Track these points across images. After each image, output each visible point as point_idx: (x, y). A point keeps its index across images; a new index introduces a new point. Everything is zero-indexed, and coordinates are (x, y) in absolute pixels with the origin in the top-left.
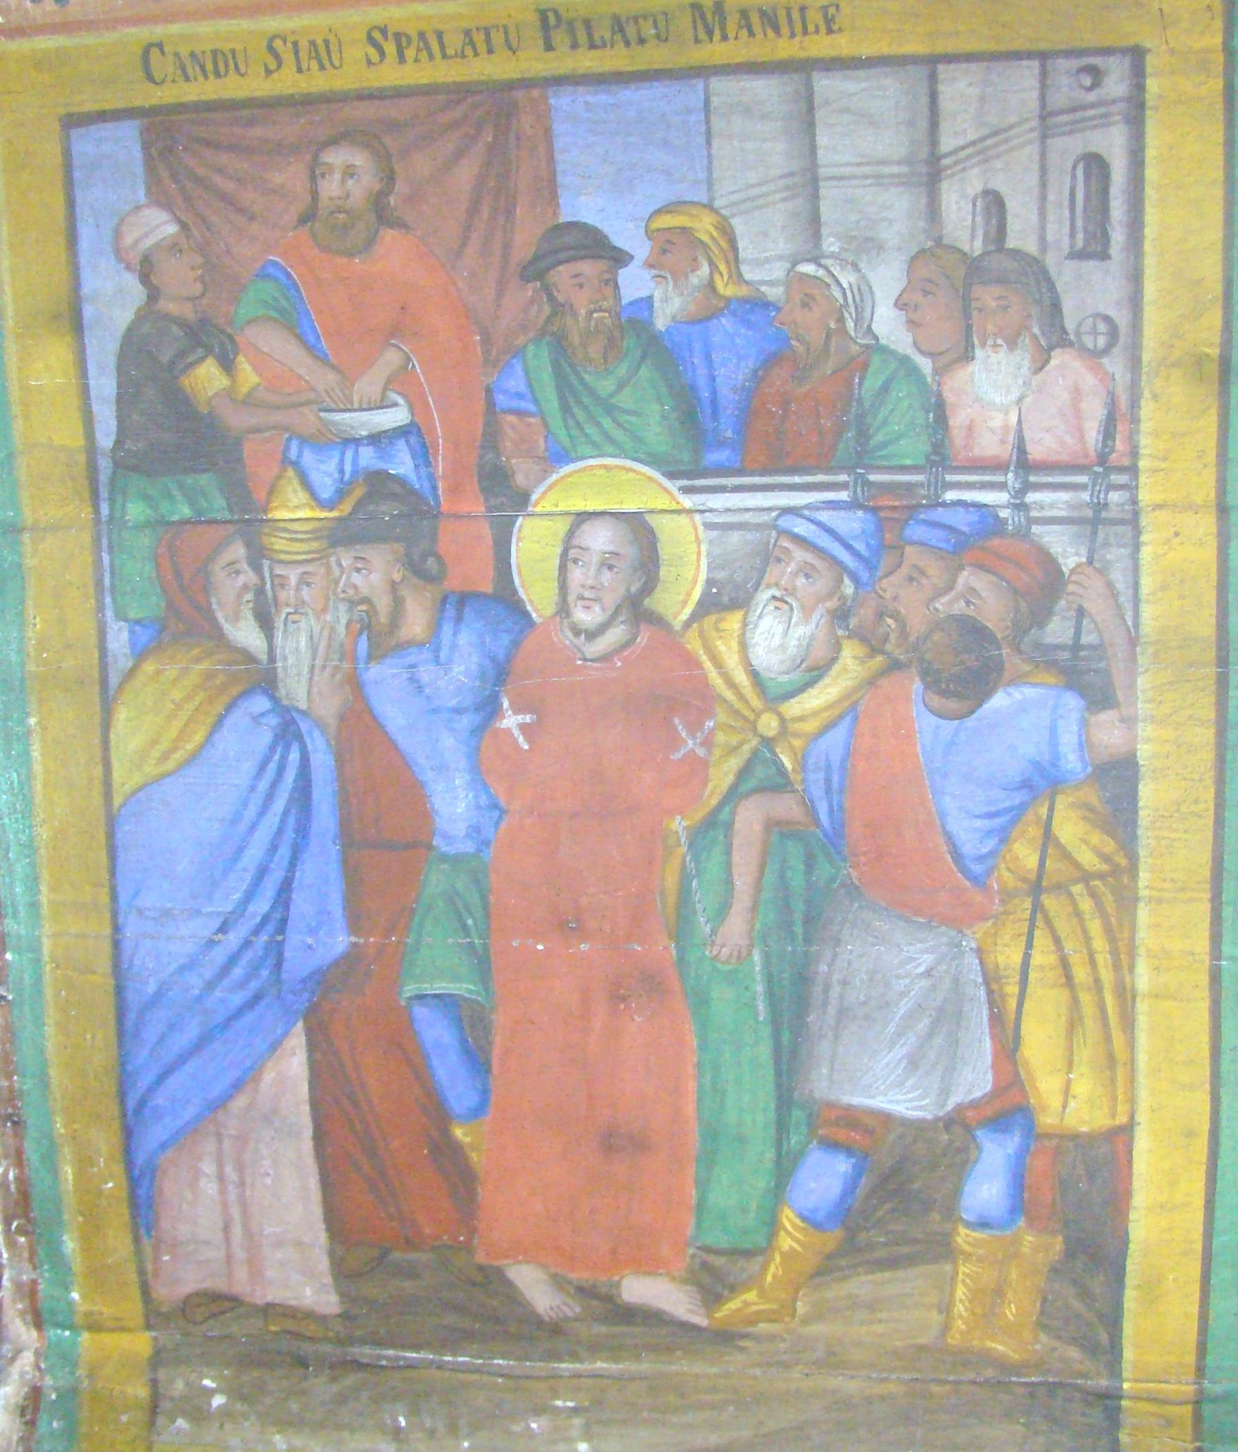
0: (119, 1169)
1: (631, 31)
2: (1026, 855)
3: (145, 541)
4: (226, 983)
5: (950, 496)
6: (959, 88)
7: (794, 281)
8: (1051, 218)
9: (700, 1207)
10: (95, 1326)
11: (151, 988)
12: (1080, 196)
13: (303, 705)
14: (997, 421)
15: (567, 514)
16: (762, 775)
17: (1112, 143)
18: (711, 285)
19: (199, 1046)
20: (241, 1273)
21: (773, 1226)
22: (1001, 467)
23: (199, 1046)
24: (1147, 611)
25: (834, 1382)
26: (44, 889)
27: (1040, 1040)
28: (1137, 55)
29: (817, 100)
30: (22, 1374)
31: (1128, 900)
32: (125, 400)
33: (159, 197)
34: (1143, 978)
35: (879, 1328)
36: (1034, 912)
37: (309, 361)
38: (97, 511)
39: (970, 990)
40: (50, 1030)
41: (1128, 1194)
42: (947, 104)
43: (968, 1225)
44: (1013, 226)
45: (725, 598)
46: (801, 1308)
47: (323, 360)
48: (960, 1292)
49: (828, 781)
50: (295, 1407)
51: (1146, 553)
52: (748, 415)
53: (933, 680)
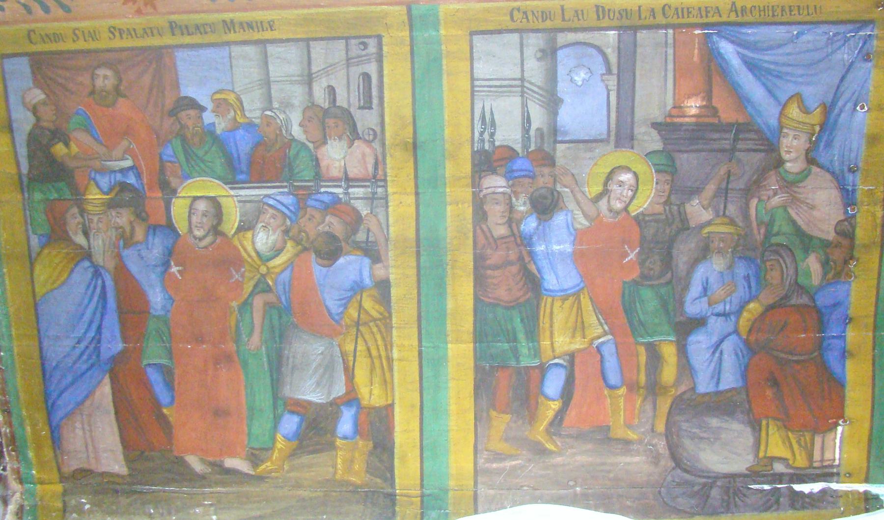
0: (47, 428)
1: (202, 30)
2: (353, 312)
3: (41, 207)
4: (81, 361)
5: (323, 190)
6: (317, 49)
7: (263, 117)
8: (351, 95)
9: (249, 434)
10: (42, 483)
11: (54, 364)
12: (361, 87)
13: (102, 264)
14: (337, 164)
15: (189, 197)
16: (262, 287)
17: (372, 69)
18: (235, 119)
19: (72, 384)
20: (93, 461)
21: (274, 439)
22: (339, 180)
23: (72, 384)
24: (392, 229)
25: (301, 492)
26: (13, 329)
27: (361, 375)
28: (379, 38)
29: (269, 54)
30: (16, 501)
31: (389, 327)
32: (31, 157)
33: (38, 84)
34: (395, 354)
35: (313, 474)
36: (357, 334)
37: (95, 143)
38: (23, 195)
39: (336, 358)
40: (19, 379)
41: (393, 428)
42: (313, 55)
43: (340, 438)
44: (338, 98)
45: (246, 226)
46: (286, 467)
47: (102, 144)
48: (339, 461)
49: (284, 289)
50: (114, 508)
51: (390, 209)
52: (251, 163)
53: (318, 254)
